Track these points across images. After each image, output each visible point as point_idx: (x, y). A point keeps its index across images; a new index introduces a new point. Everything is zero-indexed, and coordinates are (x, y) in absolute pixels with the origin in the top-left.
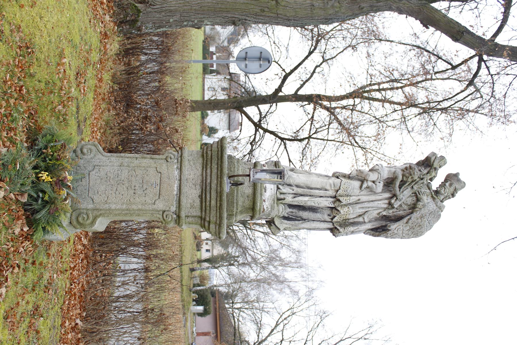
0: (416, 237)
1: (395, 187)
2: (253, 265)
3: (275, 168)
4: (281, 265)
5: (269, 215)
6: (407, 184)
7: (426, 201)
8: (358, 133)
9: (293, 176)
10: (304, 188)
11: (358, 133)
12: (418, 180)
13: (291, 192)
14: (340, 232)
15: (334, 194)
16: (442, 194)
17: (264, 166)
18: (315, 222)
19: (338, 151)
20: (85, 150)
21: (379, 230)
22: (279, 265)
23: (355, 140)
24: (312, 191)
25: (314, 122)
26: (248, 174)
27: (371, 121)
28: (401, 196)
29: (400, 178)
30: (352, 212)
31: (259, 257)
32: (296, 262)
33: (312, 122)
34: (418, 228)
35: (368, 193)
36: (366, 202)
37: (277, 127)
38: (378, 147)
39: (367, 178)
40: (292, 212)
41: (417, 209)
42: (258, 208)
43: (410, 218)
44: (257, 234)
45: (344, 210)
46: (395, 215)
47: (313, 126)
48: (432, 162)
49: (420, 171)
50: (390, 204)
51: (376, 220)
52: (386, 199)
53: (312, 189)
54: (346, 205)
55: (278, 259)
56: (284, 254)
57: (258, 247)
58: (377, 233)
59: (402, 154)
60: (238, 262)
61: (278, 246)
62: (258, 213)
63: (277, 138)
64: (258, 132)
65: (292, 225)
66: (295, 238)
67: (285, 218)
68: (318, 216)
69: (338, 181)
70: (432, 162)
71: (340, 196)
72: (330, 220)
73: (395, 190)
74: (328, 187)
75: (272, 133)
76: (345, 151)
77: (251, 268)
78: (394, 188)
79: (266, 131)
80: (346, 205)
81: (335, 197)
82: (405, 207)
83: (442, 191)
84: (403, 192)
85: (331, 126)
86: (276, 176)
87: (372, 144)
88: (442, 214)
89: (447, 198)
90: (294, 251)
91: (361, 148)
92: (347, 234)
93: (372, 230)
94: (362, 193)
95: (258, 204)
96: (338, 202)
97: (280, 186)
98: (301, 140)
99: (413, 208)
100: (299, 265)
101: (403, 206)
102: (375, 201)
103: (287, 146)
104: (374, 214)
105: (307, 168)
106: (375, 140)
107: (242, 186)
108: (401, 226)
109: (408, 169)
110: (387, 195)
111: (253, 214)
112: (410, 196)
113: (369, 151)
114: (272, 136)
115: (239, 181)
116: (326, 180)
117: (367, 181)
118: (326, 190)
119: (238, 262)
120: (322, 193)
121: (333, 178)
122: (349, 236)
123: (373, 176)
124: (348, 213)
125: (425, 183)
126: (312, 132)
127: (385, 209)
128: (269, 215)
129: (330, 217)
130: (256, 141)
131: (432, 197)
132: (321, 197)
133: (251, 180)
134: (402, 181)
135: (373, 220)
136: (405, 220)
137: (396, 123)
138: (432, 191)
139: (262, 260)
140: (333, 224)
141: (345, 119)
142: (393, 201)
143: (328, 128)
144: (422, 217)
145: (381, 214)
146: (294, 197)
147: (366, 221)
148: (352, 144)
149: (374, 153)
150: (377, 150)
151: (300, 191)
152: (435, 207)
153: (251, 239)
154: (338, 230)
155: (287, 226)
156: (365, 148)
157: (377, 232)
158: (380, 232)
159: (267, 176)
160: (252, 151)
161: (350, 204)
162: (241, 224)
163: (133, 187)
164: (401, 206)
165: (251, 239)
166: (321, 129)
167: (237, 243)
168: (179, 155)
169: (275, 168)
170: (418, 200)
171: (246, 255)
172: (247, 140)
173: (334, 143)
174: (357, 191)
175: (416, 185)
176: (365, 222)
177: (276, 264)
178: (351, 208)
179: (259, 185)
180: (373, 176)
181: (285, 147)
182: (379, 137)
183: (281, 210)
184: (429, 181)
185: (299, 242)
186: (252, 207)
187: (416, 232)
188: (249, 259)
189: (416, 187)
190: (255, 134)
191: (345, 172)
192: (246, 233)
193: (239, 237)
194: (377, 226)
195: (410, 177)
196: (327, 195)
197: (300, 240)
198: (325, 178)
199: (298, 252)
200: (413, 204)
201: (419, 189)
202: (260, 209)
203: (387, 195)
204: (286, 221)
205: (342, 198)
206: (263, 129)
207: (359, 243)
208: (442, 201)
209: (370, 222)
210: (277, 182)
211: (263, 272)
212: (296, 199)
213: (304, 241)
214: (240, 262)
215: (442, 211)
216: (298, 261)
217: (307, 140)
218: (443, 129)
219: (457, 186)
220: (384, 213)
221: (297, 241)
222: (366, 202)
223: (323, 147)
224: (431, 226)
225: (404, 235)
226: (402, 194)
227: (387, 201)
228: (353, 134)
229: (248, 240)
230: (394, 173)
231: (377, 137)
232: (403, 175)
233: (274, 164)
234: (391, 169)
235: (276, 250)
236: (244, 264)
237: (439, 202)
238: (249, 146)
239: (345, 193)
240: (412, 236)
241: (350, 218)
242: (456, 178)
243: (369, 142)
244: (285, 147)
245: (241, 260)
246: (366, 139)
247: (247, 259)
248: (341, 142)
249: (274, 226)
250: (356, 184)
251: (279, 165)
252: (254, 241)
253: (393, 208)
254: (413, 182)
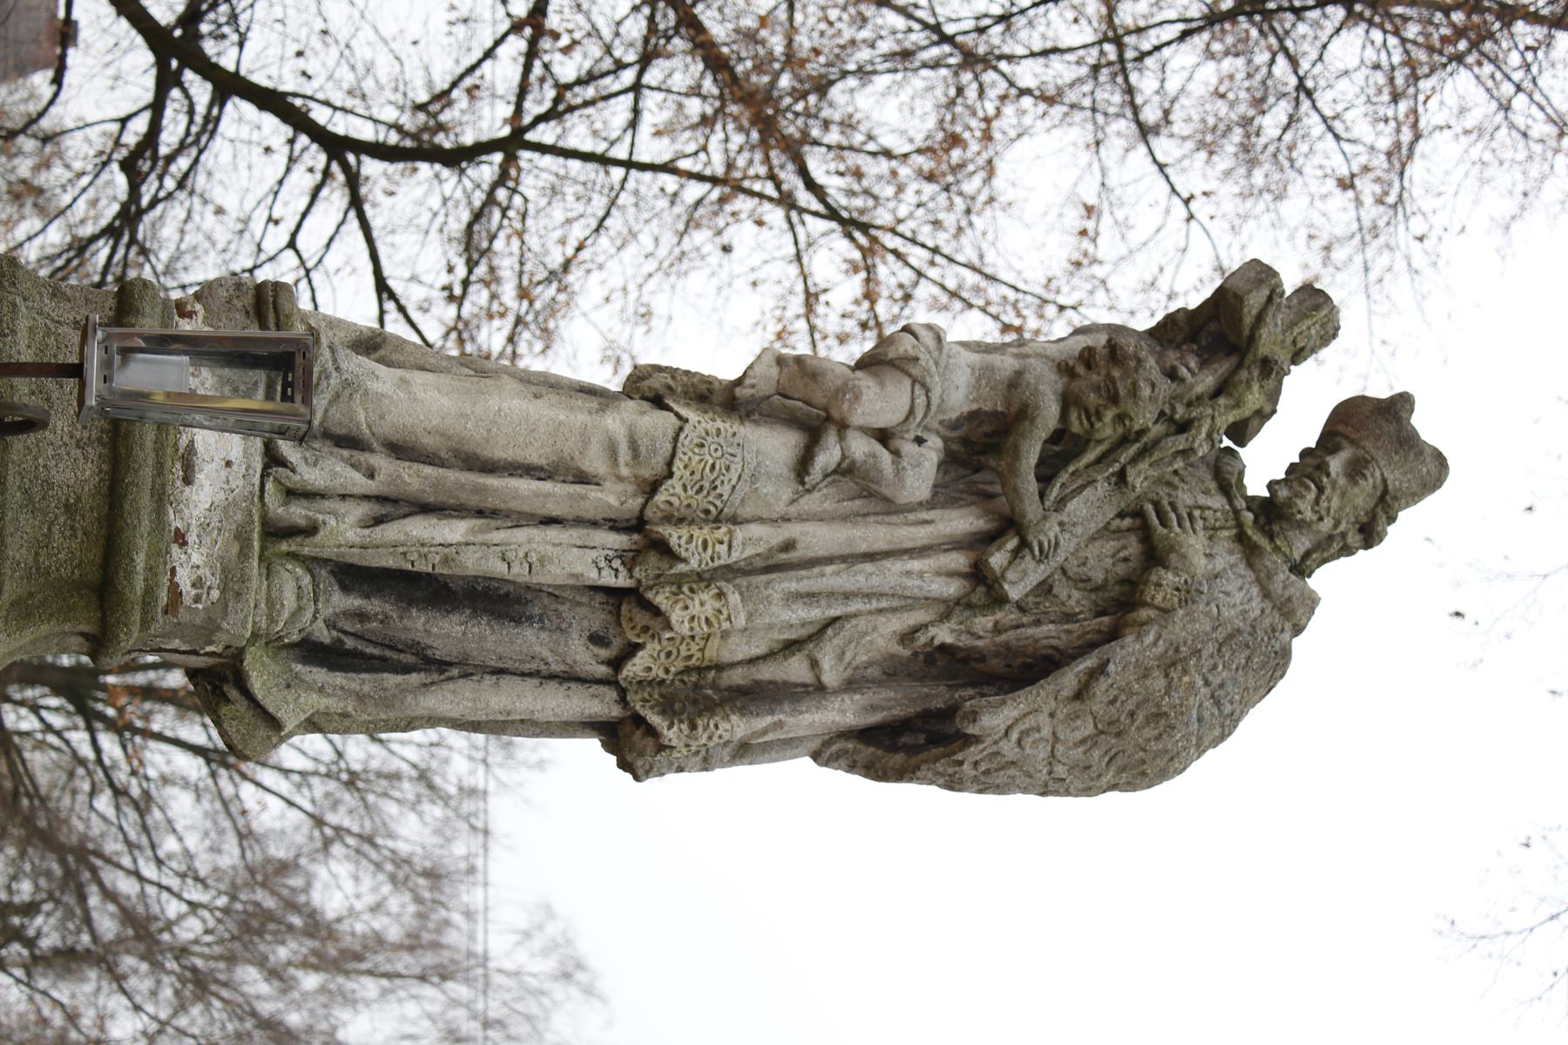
0: (1131, 786)
1: (1013, 470)
2: (128, 962)
3: (254, 331)
4: (317, 962)
5: (210, 628)
6: (1090, 456)
7: (1201, 564)
8: (826, 124)
9: (374, 386)
10: (442, 464)
11: (826, 124)
12: (1156, 430)
13: (357, 481)
14: (661, 748)
15: (635, 503)
16: (1302, 525)
17: (182, 309)
18: (506, 681)
19: (700, 237)
21: (905, 739)
22: (305, 965)
23: (803, 172)
24: (492, 481)
25: (546, 43)
26: (74, 359)
27: (906, 54)
28: (1051, 529)
29: (1049, 414)
30: (741, 621)
31: (173, 908)
32: (413, 944)
33: (533, 43)
34: (1149, 732)
35: (849, 506)
36: (829, 560)
37: (301, 63)
38: (949, 220)
40: (362, 616)
41: (1144, 613)
42: (139, 584)
43: (1100, 670)
44: (159, 758)
45: (695, 608)
46: (1007, 646)
47: (538, 69)
48: (1248, 320)
49: (1172, 375)
50: (979, 575)
51: (892, 671)
52: (956, 545)
53: (490, 467)
54: (704, 579)
55: (296, 921)
56: (339, 889)
57: (169, 845)
58: (898, 759)
59: (1097, 270)
60: (30, 943)
61: (300, 839)
62: (136, 616)
63: (303, 140)
64: (175, 93)
65: (361, 698)
66: (408, 789)
67: (311, 652)
68: (531, 641)
69: (657, 423)
70: (1248, 320)
71: (668, 519)
72: (603, 671)
73: (1014, 493)
74: (595, 463)
75: (270, 100)
76: (743, 234)
77: (118, 979)
78: (1007, 477)
79: (229, 85)
80: (704, 579)
81: (637, 525)
82: (1074, 598)
83: (1305, 508)
84: (1061, 503)
85: (653, 76)
86: (260, 376)
87: (909, 196)
88: (1297, 644)
89: (1334, 547)
90: (401, 871)
91: (842, 221)
92: (706, 764)
93: (865, 735)
94: (810, 503)
95: (140, 560)
96: (653, 558)
97: (286, 448)
98: (458, 158)
99: (1122, 604)
100: (429, 959)
101: (1062, 590)
102: (887, 554)
103: (373, 192)
104: (882, 636)
105: (492, 338)
106: (930, 177)
107: (31, 438)
108: (1043, 718)
109: (1102, 360)
110: (963, 521)
111: (104, 623)
112: (1106, 531)
113: (890, 241)
114: (269, 121)
115: (13, 407)
116: (580, 418)
117: (843, 427)
118: (582, 478)
119: (30, 943)
120: (554, 495)
121: (631, 405)
122: (719, 774)
123: (882, 402)
124: (715, 629)
125: (1203, 450)
126: (532, 108)
127: (948, 609)
128: (210, 628)
129: (604, 653)
130: (164, 150)
131: (1241, 538)
132: (549, 521)
133: (92, 401)
134: (1058, 436)
135: (874, 672)
136: (1069, 679)
137: (1060, 71)
138: (1241, 504)
139: (191, 928)
140: (623, 693)
141: (751, 37)
142: (997, 559)
143: (636, 88)
144: (1172, 663)
145: (922, 639)
146: (378, 521)
147: (830, 677)
148: (786, 201)
149: (917, 256)
150: (942, 239)
151: (414, 478)
152: (1256, 605)
153: (119, 792)
154: (652, 732)
155: (323, 703)
156: (865, 228)
157: (893, 749)
158: (912, 750)
159: (205, 381)
160: (130, 215)
161: (731, 572)
162: (57, 691)
164: (1044, 589)
165: (119, 792)
166: (590, 92)
167: (28, 821)
169: (254, 331)
170: (1154, 555)
171: (82, 898)
172: (97, 138)
173: (670, 182)
174: (777, 492)
175: (1143, 466)
176: (820, 688)
177: (283, 953)
178: (734, 598)
179: (150, 437)
180: (882, 402)
181: (356, 203)
182: (956, 154)
183: (290, 601)
184: (1227, 442)
185: (436, 811)
186: (94, 575)
187: (1138, 749)
188: (107, 925)
189: (1140, 478)
190: (157, 107)
191: (706, 370)
192: (86, 751)
193: (43, 779)
194: (897, 712)
195: (1109, 415)
196: (589, 511)
197: (446, 799)
198: (580, 401)
199: (434, 875)
200: (1122, 581)
201: (1163, 491)
202: (149, 591)
203: (963, 521)
204: (319, 675)
205: (684, 532)
206: (209, 70)
207: (788, 830)
208: (1302, 569)
210: (267, 422)
211: (196, 1010)
212: (391, 532)
213: (467, 806)
214: (45, 943)
215: (1298, 630)
216: (426, 937)
217: (498, 157)
218: (1359, 124)
219: (1395, 478)
220: (944, 634)
221: (426, 807)
222: (829, 560)
223: (599, 204)
224: (1226, 726)
225: (1060, 770)
226: (1055, 518)
227: (959, 561)
228: (791, 130)
229: (104, 802)
230: (1015, 382)
231: (946, 156)
232: (1067, 401)
233: (248, 300)
234: (996, 359)
235: (284, 868)
236: (67, 960)
237: (1283, 574)
238: (120, 181)
239: (701, 501)
240: (1109, 777)
241: (726, 657)
242: (1392, 428)
243: (889, 191)
244: (356, 203)
245: (48, 930)
246: (876, 168)
247: (88, 921)
248: (714, 180)
249: (241, 705)
250: (774, 446)
251: (285, 307)
252: (143, 805)
253: (1000, 600)
254: (1124, 441)
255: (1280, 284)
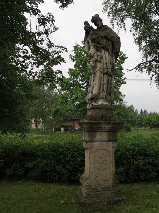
20: (88, 185)
24: (105, 82)
29: (96, 44)
39: (96, 59)
51: (112, 57)
74: (100, 77)
81: (104, 74)
84: (102, 43)
94: (102, 62)
117: (97, 59)
147: (112, 61)
163: (103, 161)
168: (89, 142)
209: (113, 59)
255: (73, 69)
